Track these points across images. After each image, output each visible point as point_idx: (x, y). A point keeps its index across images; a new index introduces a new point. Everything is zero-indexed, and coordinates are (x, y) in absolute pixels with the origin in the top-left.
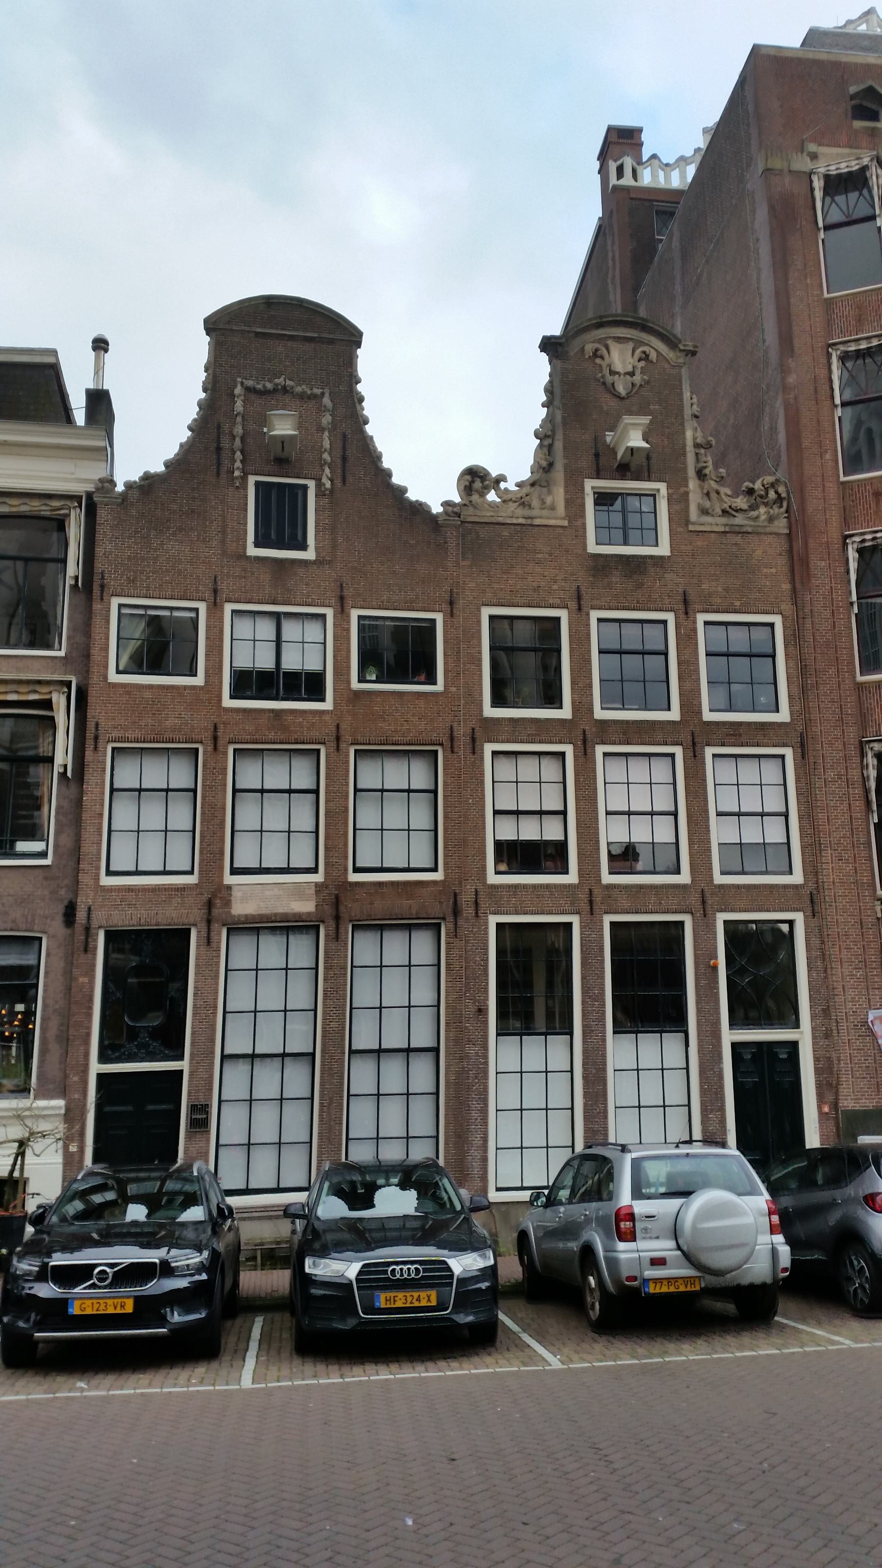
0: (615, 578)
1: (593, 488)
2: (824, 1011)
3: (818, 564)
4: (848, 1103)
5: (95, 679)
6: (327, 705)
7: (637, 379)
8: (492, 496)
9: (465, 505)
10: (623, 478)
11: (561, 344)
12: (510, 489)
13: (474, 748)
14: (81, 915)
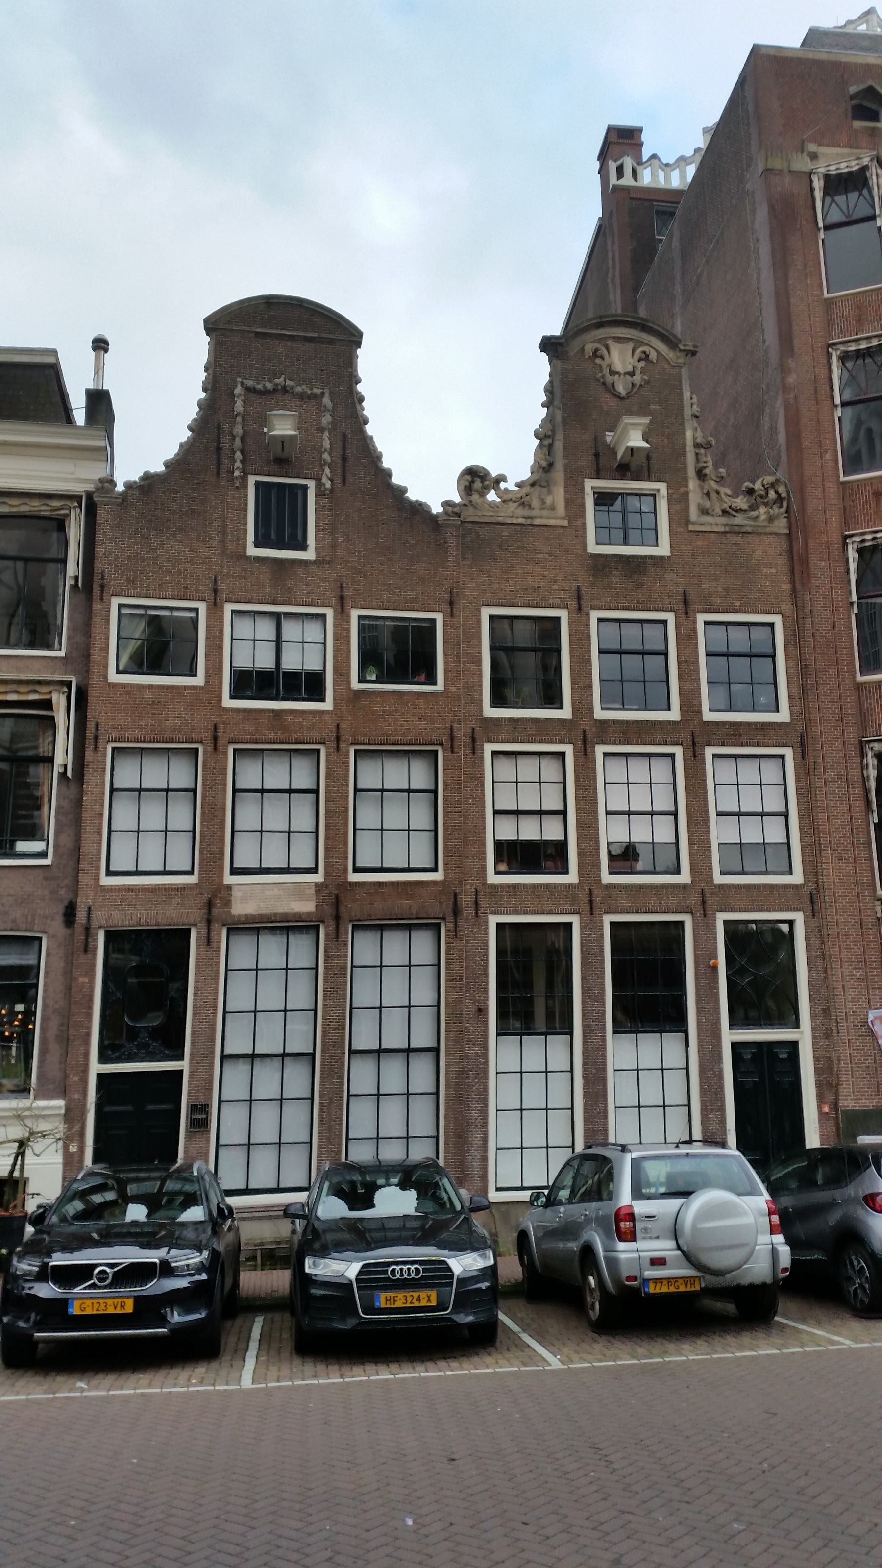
0: (615, 578)
1: (593, 488)
2: (824, 1011)
3: (818, 564)
4: (848, 1103)
5: (95, 679)
6: (327, 705)
7: (637, 379)
8: (492, 496)
9: (465, 505)
10: (623, 478)
11: (561, 344)
12: (510, 489)
13: (474, 748)
14: (81, 915)
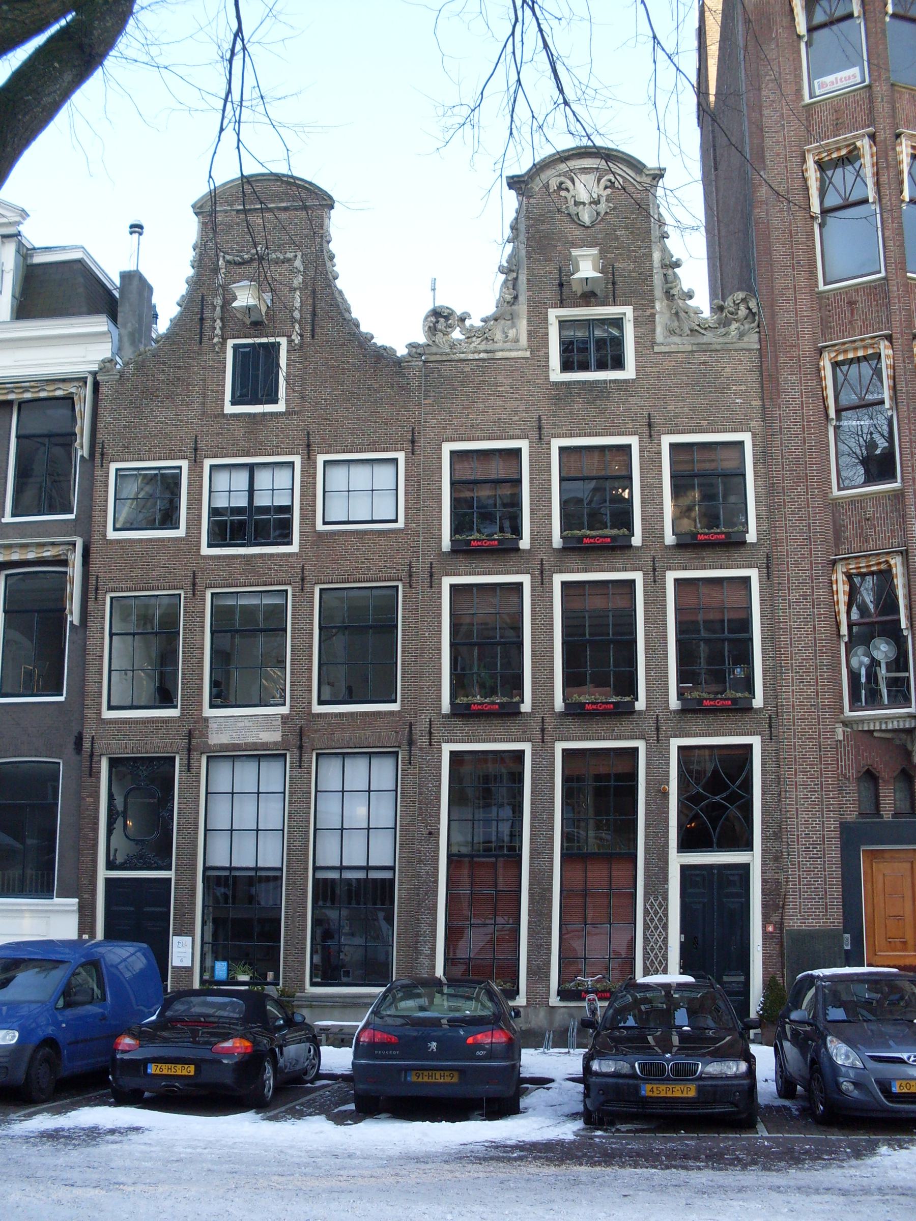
0: (578, 406)
1: (557, 317)
2: (774, 834)
3: (789, 378)
4: (794, 922)
5: (96, 537)
6: (294, 548)
7: (603, 207)
8: (457, 334)
10: (588, 304)
12: (475, 325)
13: (431, 582)
14: (87, 745)
